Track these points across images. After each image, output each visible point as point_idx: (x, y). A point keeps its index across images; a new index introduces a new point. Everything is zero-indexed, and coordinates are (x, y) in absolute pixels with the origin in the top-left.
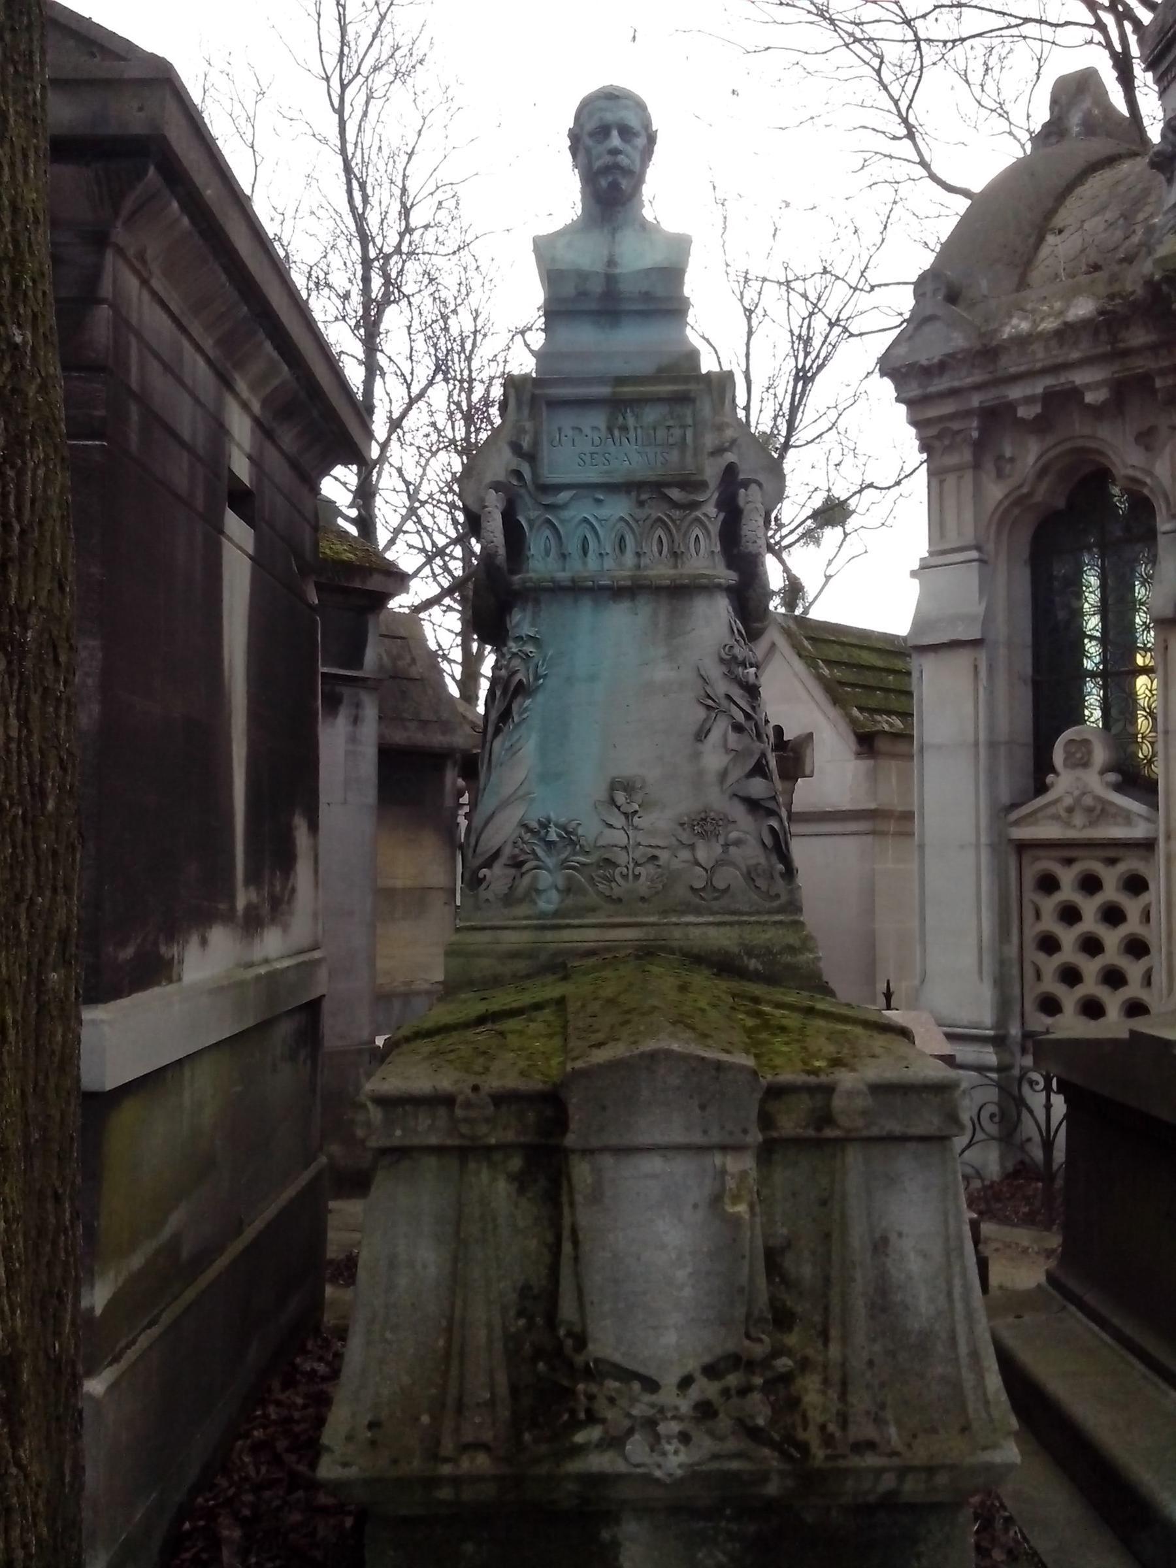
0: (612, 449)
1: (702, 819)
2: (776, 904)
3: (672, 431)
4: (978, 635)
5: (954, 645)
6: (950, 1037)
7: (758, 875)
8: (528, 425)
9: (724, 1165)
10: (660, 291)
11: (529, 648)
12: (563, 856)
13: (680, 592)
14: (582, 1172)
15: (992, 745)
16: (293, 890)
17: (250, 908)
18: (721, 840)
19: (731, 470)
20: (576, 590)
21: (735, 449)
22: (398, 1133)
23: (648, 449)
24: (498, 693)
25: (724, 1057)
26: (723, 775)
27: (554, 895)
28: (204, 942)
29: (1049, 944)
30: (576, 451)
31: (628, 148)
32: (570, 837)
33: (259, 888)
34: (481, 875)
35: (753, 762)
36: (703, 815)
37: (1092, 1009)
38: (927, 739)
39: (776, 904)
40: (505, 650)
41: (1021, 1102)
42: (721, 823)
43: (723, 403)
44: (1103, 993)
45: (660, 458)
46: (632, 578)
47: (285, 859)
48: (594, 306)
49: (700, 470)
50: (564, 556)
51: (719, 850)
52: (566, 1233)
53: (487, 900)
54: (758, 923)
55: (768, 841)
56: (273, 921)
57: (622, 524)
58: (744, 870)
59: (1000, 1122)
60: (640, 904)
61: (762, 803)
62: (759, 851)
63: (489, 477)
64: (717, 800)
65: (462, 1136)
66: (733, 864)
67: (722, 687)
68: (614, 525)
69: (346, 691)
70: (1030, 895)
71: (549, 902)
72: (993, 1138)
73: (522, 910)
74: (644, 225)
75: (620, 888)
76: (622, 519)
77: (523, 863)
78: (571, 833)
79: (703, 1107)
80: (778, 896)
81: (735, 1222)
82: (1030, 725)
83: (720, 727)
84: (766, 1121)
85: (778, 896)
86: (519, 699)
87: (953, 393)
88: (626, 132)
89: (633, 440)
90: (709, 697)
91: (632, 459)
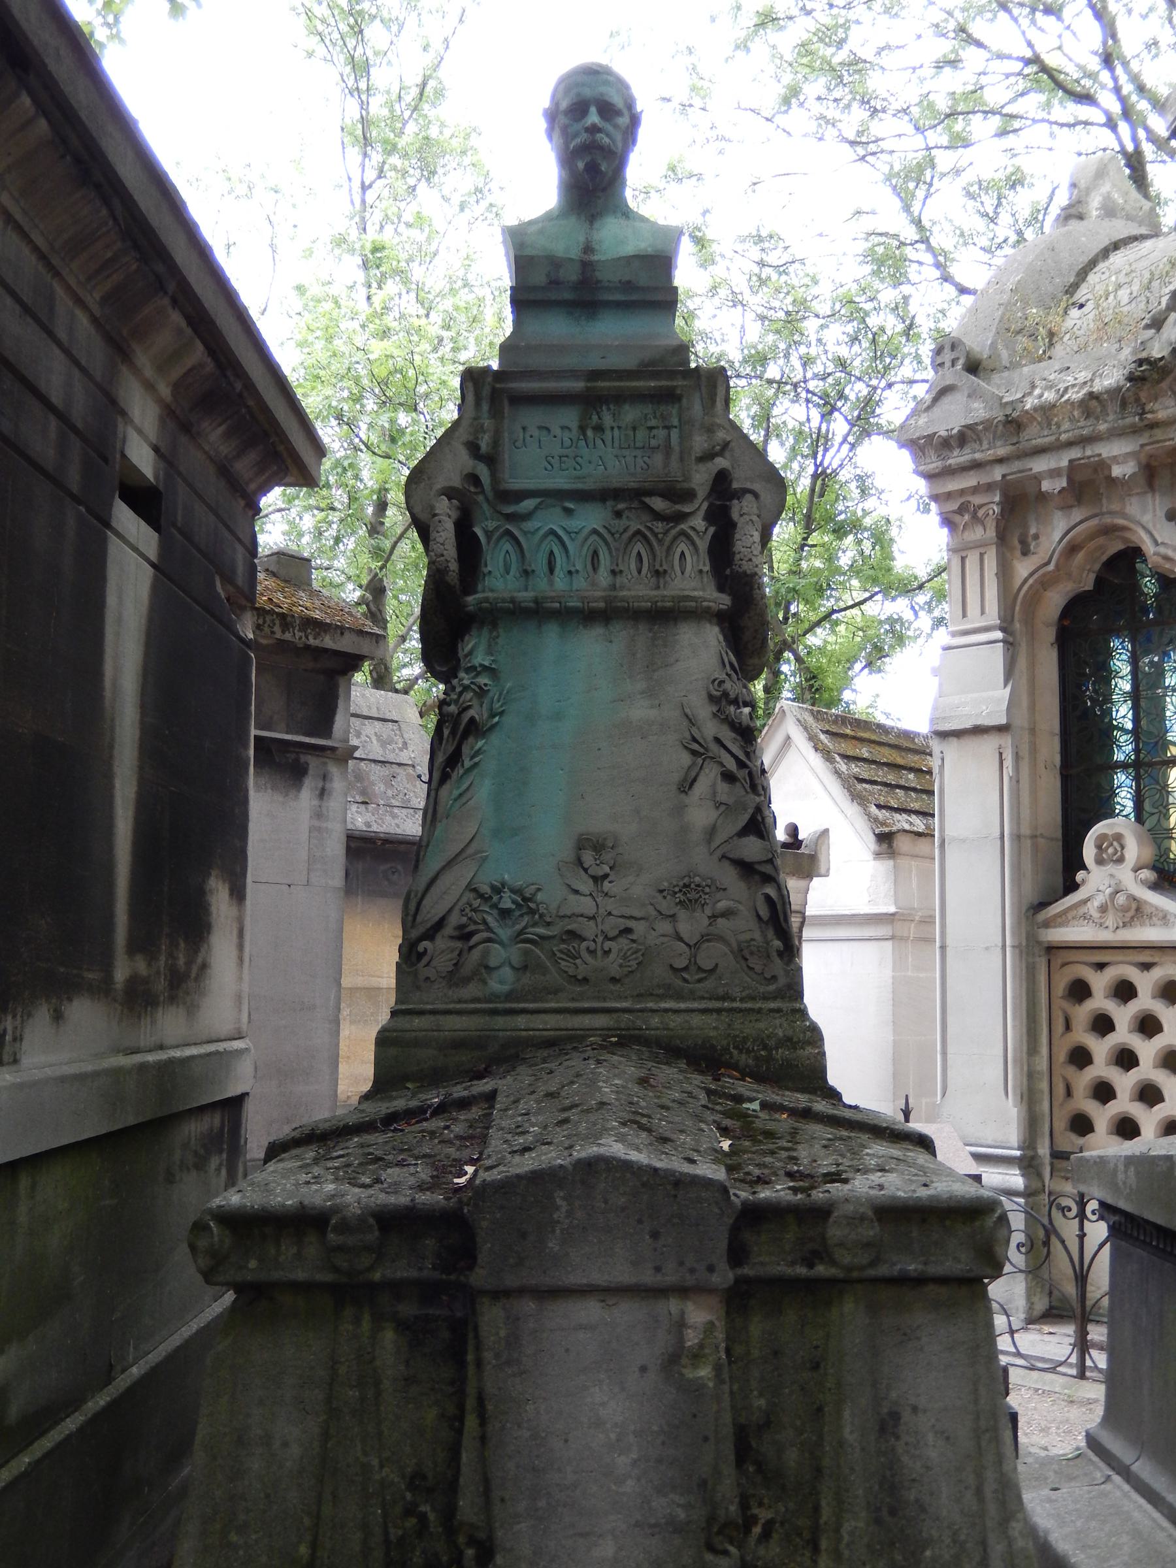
0: (585, 451)
1: (685, 886)
2: (772, 988)
3: (655, 432)
4: (1004, 721)
5: (979, 731)
6: (978, 1157)
7: (752, 953)
8: (487, 423)
9: (683, 1313)
10: (643, 280)
11: (483, 680)
12: (518, 927)
13: (664, 616)
14: (492, 1319)
15: (1017, 838)
16: (204, 966)
17: (133, 981)
18: (708, 911)
19: (722, 479)
20: (538, 613)
21: (727, 454)
22: (253, 1264)
23: (626, 452)
24: (446, 732)
25: (687, 1168)
26: (711, 832)
27: (507, 972)
28: (58, 1017)
29: (1081, 1057)
30: (541, 453)
31: (608, 127)
32: (526, 902)
33: (152, 958)
34: (420, 948)
35: (746, 817)
36: (686, 880)
37: (1127, 1128)
38: (949, 832)
39: (772, 988)
40: (455, 682)
41: (1051, 1231)
42: (707, 890)
43: (713, 401)
44: (1137, 1111)
45: (640, 461)
46: (605, 599)
47: (194, 926)
48: (567, 295)
49: (687, 479)
50: (526, 573)
51: (706, 922)
52: (470, 1403)
53: (428, 978)
54: (752, 1010)
55: (764, 912)
56: (172, 999)
57: (595, 537)
58: (735, 945)
59: (1027, 1253)
60: (612, 987)
61: (757, 867)
62: (753, 924)
63: (440, 483)
64: (704, 864)
65: (336, 1269)
66: (721, 939)
67: (710, 728)
68: (586, 539)
69: (313, 762)
70: (1061, 1004)
71: (501, 982)
72: (1021, 1271)
73: (472, 990)
74: (627, 213)
75: (586, 965)
76: (595, 531)
77: (470, 935)
78: (530, 900)
79: (655, 1235)
80: (774, 978)
81: (694, 1390)
82: (1059, 818)
83: (709, 777)
84: (737, 1254)
85: (774, 978)
86: (471, 740)
87: (976, 466)
88: (607, 110)
89: (609, 442)
90: (695, 740)
91: (609, 461)
